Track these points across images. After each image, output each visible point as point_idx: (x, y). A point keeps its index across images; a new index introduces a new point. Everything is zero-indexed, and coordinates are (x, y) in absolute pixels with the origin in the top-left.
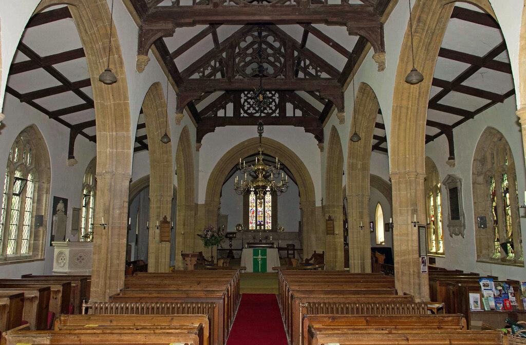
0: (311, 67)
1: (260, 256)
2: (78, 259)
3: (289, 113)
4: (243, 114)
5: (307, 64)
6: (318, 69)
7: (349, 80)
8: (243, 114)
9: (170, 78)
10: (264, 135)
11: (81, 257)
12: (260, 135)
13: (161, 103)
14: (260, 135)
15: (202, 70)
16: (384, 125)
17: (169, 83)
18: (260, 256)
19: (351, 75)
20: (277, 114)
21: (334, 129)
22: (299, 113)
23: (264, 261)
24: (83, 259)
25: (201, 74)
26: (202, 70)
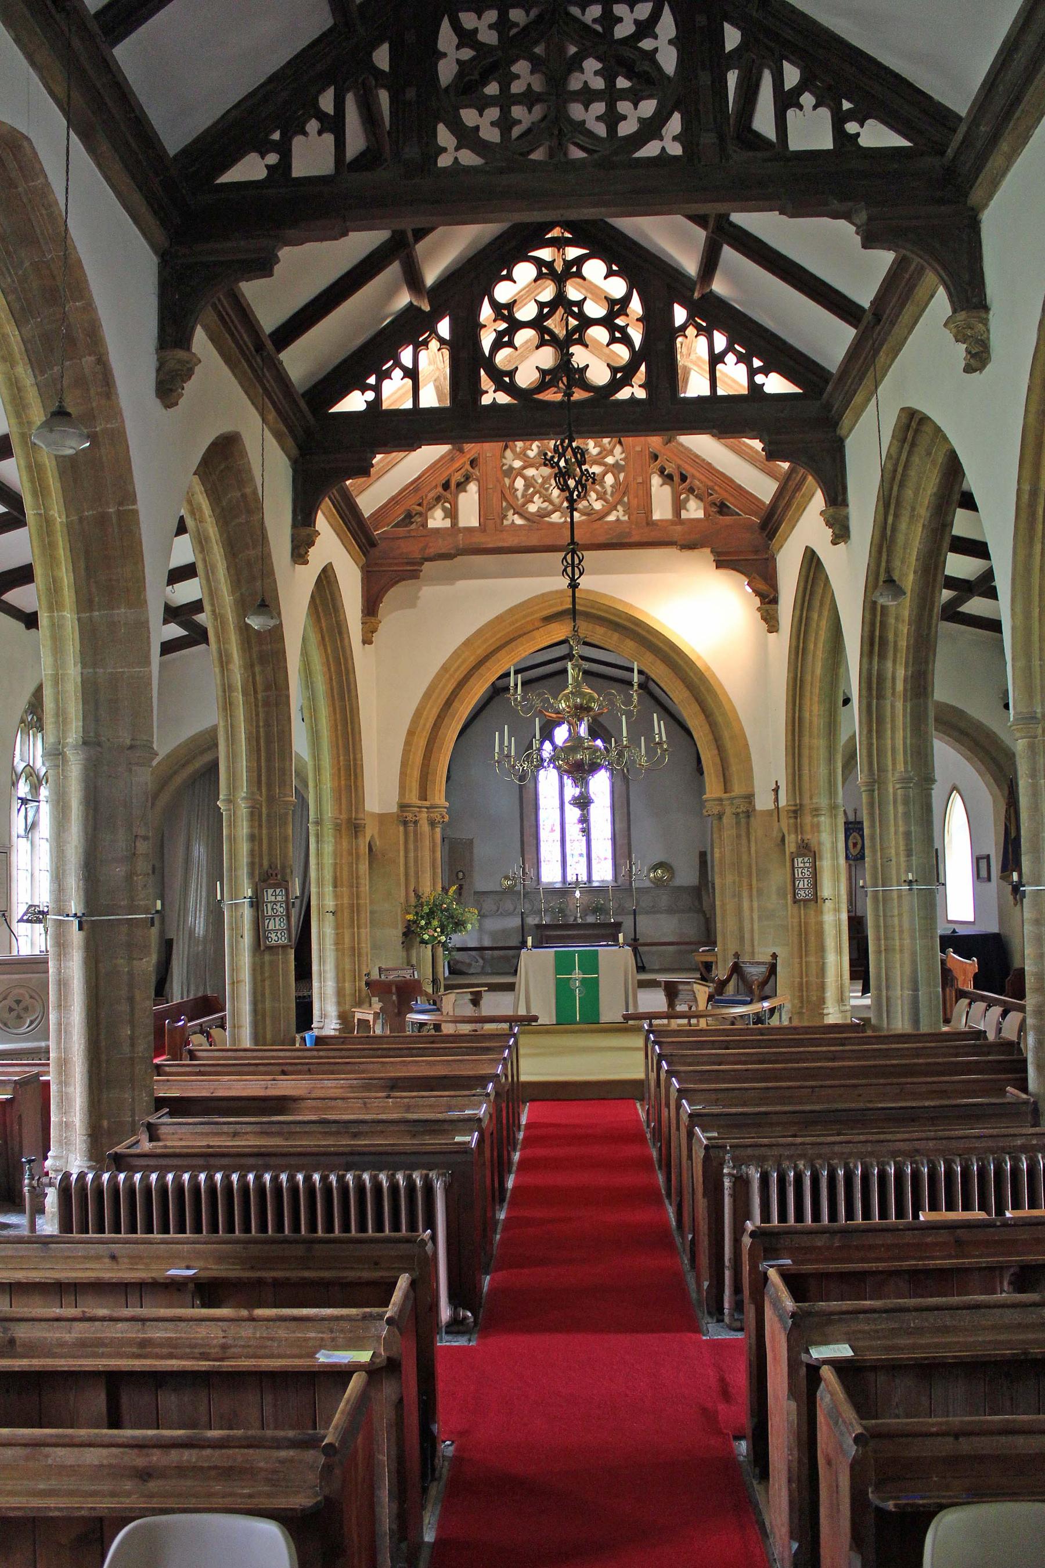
0: (730, 358)
1: (577, 975)
2: (11, 1010)
3: (661, 509)
4: (491, 396)
5: (788, 86)
6: (846, 105)
7: (858, 399)
8: (491, 396)
9: (272, 415)
10: (584, 582)
11: (18, 1002)
12: (574, 585)
13: (244, 496)
14: (574, 585)
15: (276, 136)
16: (985, 545)
17: (268, 434)
18: (577, 975)
19: (868, 381)
20: (635, 391)
21: (812, 561)
22: (694, 510)
23: (592, 987)
24: (26, 1009)
25: (370, 395)
26: (276, 136)
